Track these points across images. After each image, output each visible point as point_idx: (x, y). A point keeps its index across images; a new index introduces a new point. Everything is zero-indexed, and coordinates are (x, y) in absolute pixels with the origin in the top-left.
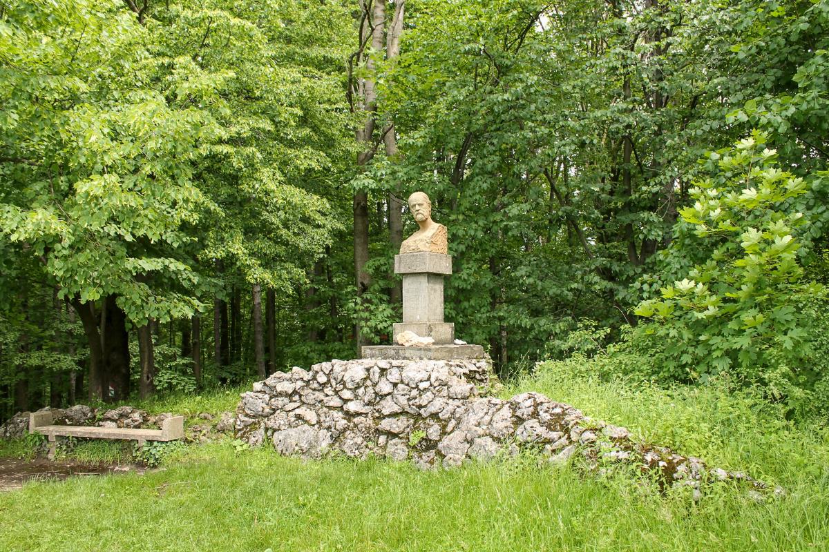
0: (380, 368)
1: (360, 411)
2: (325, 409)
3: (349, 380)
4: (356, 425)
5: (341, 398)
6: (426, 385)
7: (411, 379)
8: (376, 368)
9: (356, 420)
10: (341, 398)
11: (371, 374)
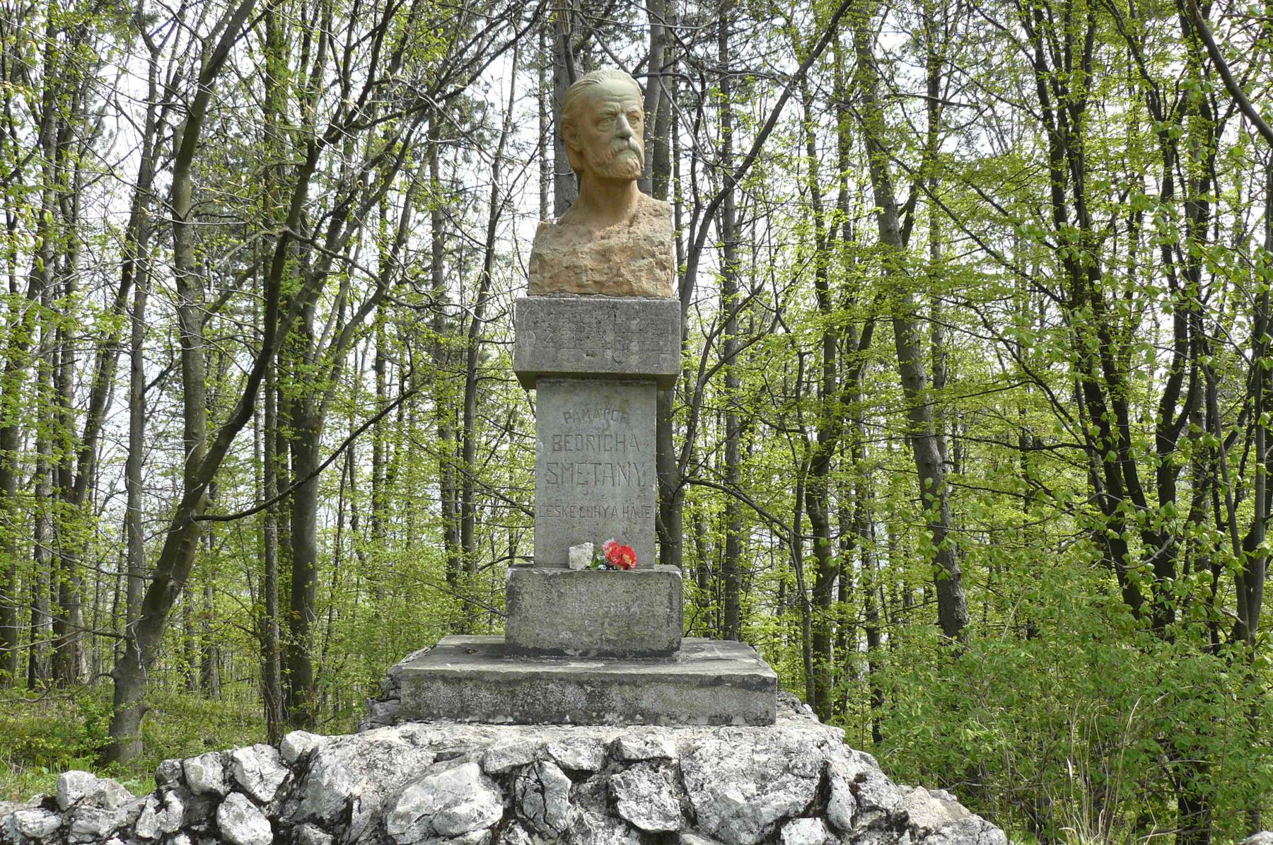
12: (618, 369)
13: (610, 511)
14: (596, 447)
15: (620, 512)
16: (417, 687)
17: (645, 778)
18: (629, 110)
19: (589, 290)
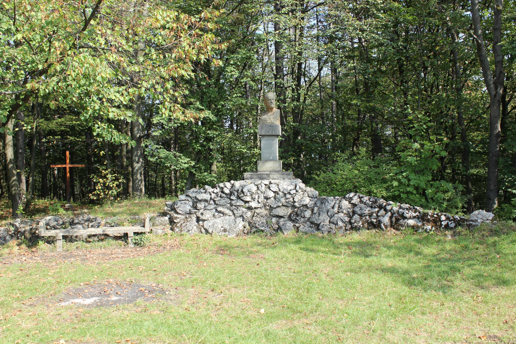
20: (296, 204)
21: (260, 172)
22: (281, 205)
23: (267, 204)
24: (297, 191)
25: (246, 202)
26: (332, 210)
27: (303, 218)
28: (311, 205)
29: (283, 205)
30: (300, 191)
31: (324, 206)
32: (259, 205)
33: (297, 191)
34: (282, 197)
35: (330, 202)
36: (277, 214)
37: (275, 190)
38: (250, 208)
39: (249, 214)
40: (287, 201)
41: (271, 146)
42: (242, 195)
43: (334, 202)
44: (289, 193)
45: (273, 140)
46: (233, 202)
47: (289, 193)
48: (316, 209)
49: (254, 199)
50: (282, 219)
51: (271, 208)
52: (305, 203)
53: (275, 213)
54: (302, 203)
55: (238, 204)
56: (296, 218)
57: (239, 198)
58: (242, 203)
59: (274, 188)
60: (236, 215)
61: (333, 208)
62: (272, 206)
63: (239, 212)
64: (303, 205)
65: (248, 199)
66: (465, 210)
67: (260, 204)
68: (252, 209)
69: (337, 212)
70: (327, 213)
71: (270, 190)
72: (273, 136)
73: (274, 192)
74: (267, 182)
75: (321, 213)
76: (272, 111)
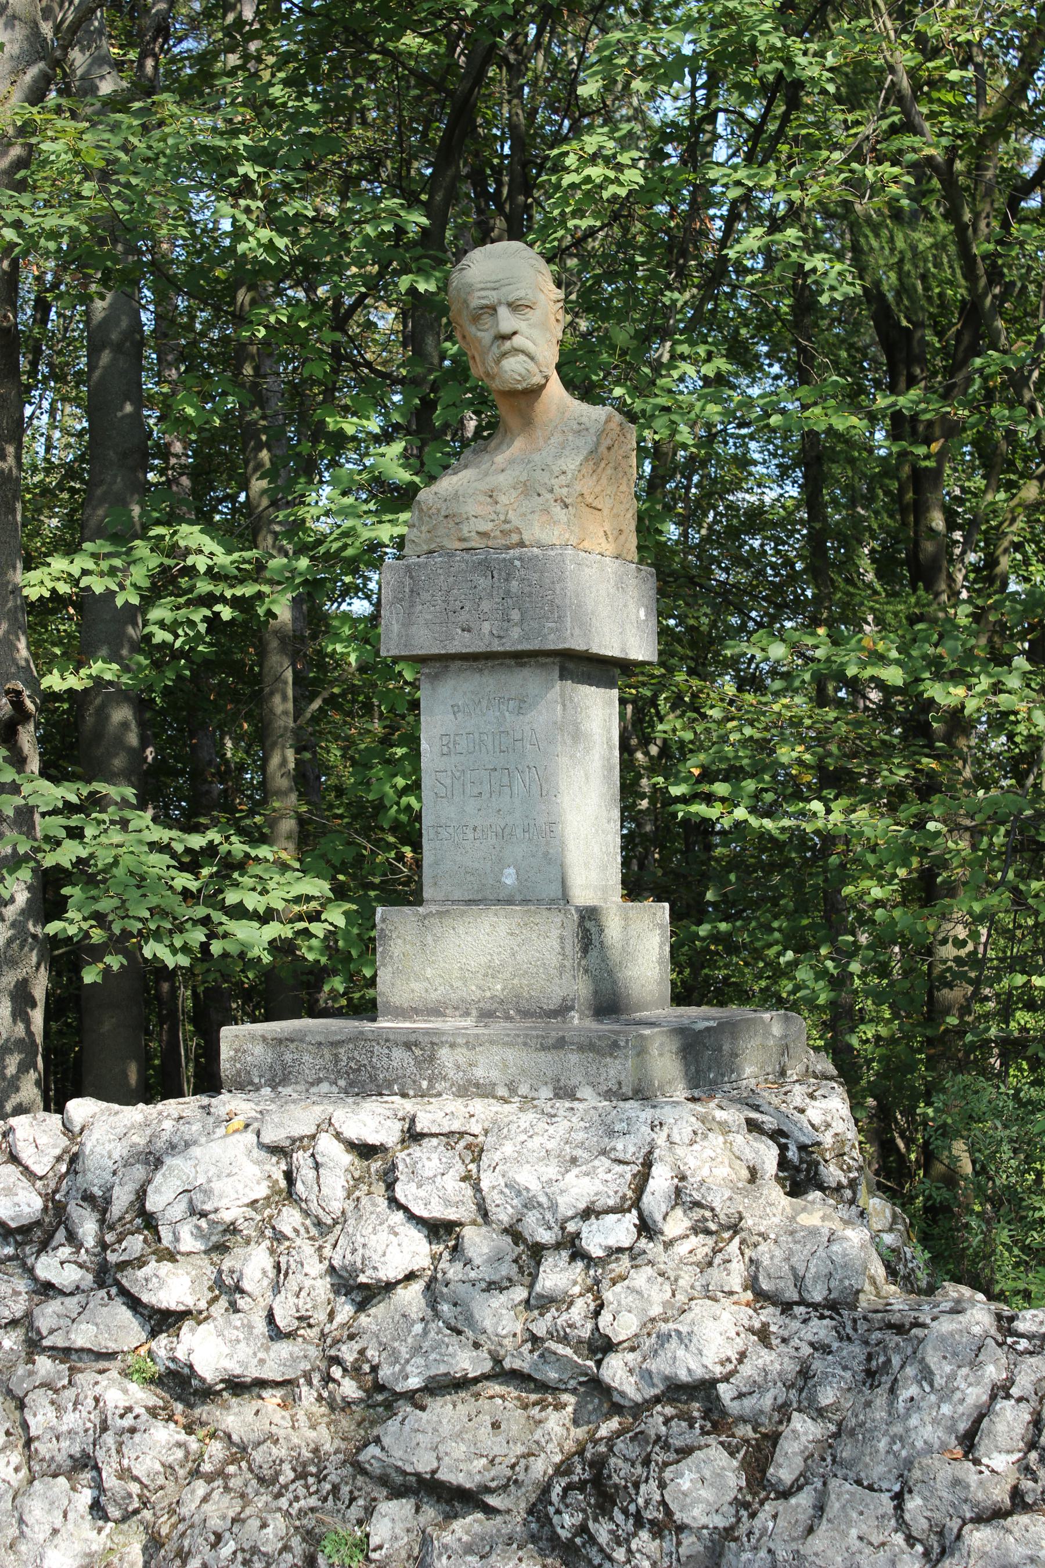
0: (352, 1146)
1: (254, 1372)
2: (44, 1364)
3: (179, 1210)
4: (239, 1451)
5: (134, 1303)
6: (620, 1230)
7: (530, 1204)
8: (327, 1144)
9: (237, 1418)
10: (134, 1303)
11: (305, 1174)
12: (497, 647)
13: (507, 831)
14: (490, 747)
15: (519, 832)
16: (237, 1051)
17: (435, 1156)
18: (511, 299)
19: (473, 544)
20: (617, 1371)
21: (400, 1013)
22: (466, 1362)
23: (348, 1353)
24: (646, 1228)
25: (164, 1321)
26: (944, 1471)
27: (658, 1530)
28: (756, 1388)
29: (501, 1373)
30: (676, 1224)
31: (880, 1398)
32: (277, 1361)
33: (646, 1228)
34: (493, 1286)
35: (942, 1369)
36: (423, 1464)
37: (436, 1211)
38: (181, 1385)
39: (161, 1442)
40: (540, 1329)
41: (520, 773)
42: (135, 1244)
43: (993, 1372)
44: (572, 1247)
45: (523, 705)
46: (48, 1315)
47: (572, 1247)
48: (804, 1431)
49: (229, 1290)
50: (468, 1525)
51: (382, 1399)
52: (687, 1365)
53: (398, 1456)
54: (659, 1365)
55: (82, 1336)
56: (583, 1529)
57: (107, 1276)
58: (123, 1329)
59: (434, 1184)
60: (43, 1448)
61: (969, 1442)
62: (385, 1373)
63: (71, 1420)
64: (676, 1391)
65: (172, 1286)
66: (1012, 718)
67: (284, 1349)
68: (207, 1394)
69: (1000, 1495)
70: (899, 1498)
71: (394, 1203)
72: (520, 658)
73: (438, 1230)
74: (373, 1121)
75: (841, 1490)
76: (528, 422)
